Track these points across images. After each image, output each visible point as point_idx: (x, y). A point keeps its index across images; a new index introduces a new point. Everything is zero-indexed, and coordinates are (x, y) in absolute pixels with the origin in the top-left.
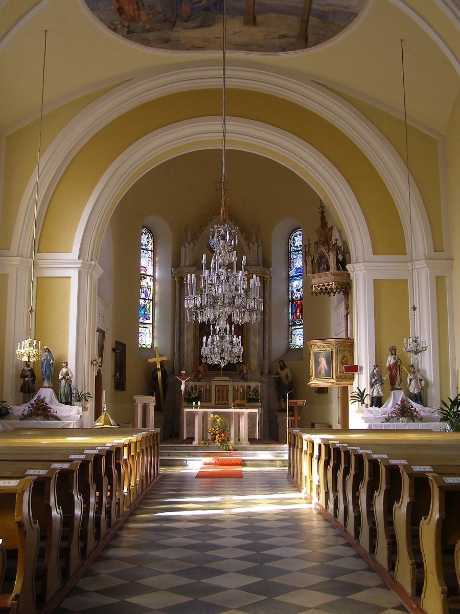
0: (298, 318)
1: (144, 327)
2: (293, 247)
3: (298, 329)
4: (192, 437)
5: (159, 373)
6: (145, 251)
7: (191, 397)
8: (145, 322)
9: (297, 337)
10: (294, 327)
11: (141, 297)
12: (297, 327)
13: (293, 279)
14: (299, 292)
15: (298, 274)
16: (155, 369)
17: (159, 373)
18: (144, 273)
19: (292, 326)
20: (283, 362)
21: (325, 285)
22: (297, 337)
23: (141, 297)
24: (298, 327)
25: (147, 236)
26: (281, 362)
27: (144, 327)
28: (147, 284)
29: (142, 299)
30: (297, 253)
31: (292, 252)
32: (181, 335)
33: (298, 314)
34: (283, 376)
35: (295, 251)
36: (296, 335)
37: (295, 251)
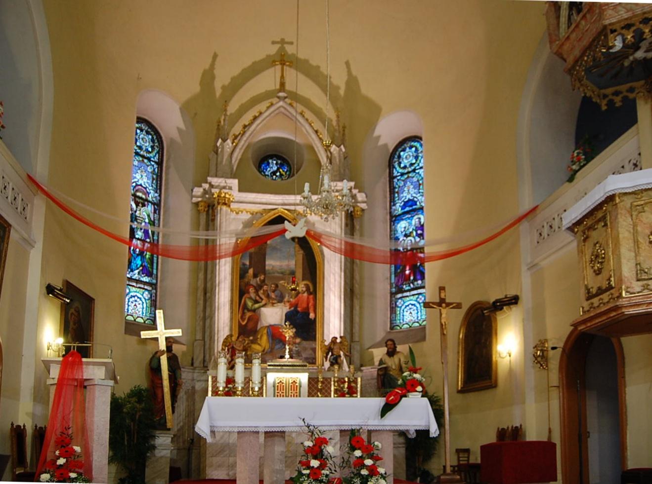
0: (407, 278)
1: (139, 288)
2: (398, 168)
3: (407, 296)
4: (219, 173)
5: (164, 360)
6: (146, 161)
7: (251, 338)
8: (142, 279)
9: (405, 310)
10: (399, 296)
11: (137, 236)
12: (405, 294)
13: (398, 218)
14: (409, 238)
15: (407, 209)
16: (156, 353)
17: (164, 360)
18: (144, 197)
19: (397, 293)
20: (394, 344)
21: (620, 92)
22: (405, 310)
23: (137, 236)
24: (408, 294)
25: (150, 137)
26: (389, 343)
27: (139, 288)
28: (149, 216)
29: (138, 239)
30: (406, 176)
31: (397, 176)
32: (208, 304)
33: (407, 272)
34: (394, 367)
35: (402, 175)
36: (403, 307)
37: (402, 175)
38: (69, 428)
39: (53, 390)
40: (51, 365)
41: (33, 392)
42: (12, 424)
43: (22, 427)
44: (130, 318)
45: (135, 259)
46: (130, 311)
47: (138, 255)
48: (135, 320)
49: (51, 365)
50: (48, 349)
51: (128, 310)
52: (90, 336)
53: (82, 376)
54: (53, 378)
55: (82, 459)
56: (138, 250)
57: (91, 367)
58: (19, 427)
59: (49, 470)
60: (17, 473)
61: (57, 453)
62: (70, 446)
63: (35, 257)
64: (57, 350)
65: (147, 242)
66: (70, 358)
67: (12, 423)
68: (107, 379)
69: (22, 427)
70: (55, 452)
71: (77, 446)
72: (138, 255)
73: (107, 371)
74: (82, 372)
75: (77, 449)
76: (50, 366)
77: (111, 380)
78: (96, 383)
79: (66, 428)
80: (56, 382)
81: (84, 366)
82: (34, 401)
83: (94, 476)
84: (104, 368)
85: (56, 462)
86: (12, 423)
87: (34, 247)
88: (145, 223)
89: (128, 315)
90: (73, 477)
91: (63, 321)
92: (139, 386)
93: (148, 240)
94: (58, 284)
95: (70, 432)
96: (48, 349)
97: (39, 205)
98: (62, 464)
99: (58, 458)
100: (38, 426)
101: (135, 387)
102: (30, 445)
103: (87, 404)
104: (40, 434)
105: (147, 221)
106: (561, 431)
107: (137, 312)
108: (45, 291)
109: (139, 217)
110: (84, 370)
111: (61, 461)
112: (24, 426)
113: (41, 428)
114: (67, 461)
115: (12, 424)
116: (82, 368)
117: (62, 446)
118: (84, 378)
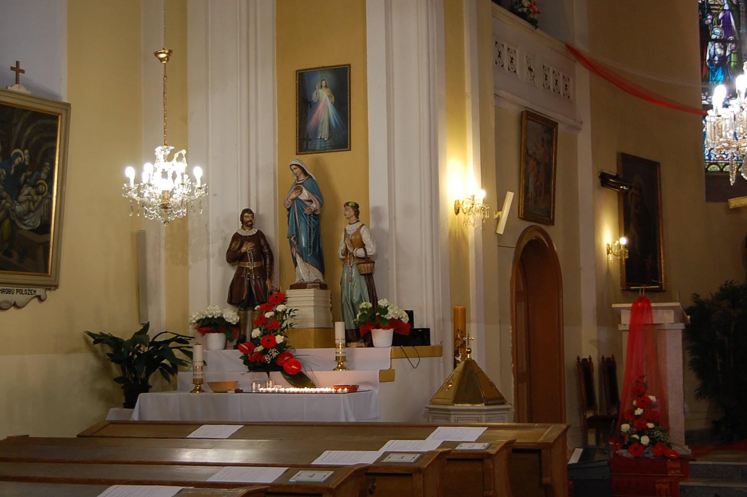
23: (714, 37)
29: (716, 40)
38: (644, 377)
39: (625, 337)
40: (622, 311)
41: (596, 313)
42: (578, 359)
43: (588, 360)
44: (714, 168)
45: (713, 74)
46: (713, 157)
47: (718, 66)
48: (722, 170)
49: (622, 311)
50: (608, 254)
51: (709, 156)
52: (658, 217)
53: (652, 321)
54: (625, 325)
55: (658, 409)
56: (716, 58)
57: (660, 311)
58: (585, 359)
59: (628, 420)
60: (588, 417)
61: (635, 403)
62: (646, 395)
63: (584, 142)
64: (619, 254)
65: (730, 41)
66: (640, 304)
67: (578, 356)
68: (678, 323)
69: (588, 360)
70: (632, 402)
71: (653, 395)
72: (718, 66)
73: (676, 314)
74: (652, 317)
75: (653, 398)
76: (620, 312)
77: (681, 322)
78: (666, 328)
79: (640, 377)
80: (628, 329)
81: (653, 311)
82: (598, 325)
83: (671, 426)
84: (672, 313)
85: (634, 412)
86: (578, 356)
87: (581, 129)
88: (724, 10)
89: (711, 164)
90: (651, 427)
91: (622, 212)
92: (731, 282)
93: (731, 38)
94: (612, 169)
95: (645, 380)
96: (608, 254)
97: (582, 74)
98: (639, 414)
99: (636, 408)
100: (606, 357)
101: (726, 285)
102: (597, 379)
103: (659, 350)
104: (609, 366)
105: (726, 7)
106: (309, 470)
107: (724, 156)
108: (598, 181)
109: (714, 5)
110: (654, 314)
111: (639, 411)
112: (590, 358)
113: (608, 359)
114: (644, 411)
115: (578, 359)
116: (651, 312)
117: (639, 396)
118: (654, 323)
